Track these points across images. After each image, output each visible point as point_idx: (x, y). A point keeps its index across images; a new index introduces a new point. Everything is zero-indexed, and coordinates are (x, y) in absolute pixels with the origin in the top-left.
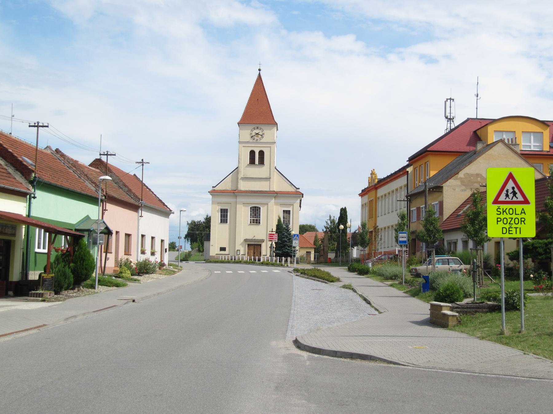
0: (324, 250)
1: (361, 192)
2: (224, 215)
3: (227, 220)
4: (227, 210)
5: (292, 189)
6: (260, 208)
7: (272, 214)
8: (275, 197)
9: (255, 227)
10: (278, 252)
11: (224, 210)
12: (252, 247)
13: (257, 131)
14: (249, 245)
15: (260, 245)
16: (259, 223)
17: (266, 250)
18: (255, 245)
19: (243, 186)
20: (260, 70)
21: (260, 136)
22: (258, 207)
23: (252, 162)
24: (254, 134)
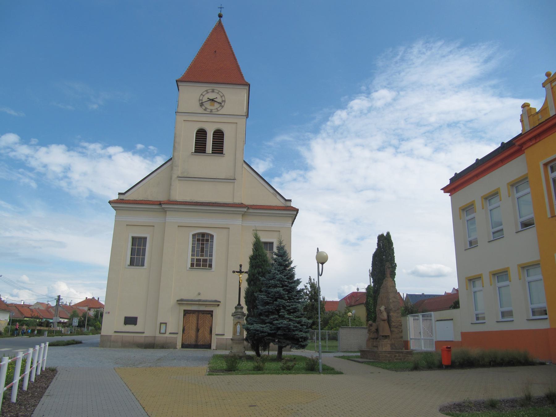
0: (389, 320)
1: (448, 183)
2: (139, 250)
3: (143, 260)
4: (145, 239)
5: (279, 203)
6: (212, 236)
7: (234, 251)
8: (244, 215)
9: (201, 274)
10: (257, 326)
11: (140, 238)
12: (193, 318)
13: (212, 96)
14: (186, 312)
15: (211, 313)
16: (210, 266)
17: (226, 326)
18: (199, 312)
19: (182, 192)
20: (220, 16)
21: (217, 105)
22: (208, 234)
23: (200, 148)
24: (205, 99)
